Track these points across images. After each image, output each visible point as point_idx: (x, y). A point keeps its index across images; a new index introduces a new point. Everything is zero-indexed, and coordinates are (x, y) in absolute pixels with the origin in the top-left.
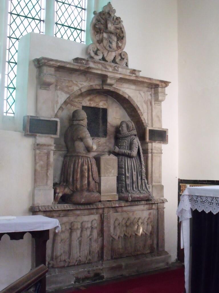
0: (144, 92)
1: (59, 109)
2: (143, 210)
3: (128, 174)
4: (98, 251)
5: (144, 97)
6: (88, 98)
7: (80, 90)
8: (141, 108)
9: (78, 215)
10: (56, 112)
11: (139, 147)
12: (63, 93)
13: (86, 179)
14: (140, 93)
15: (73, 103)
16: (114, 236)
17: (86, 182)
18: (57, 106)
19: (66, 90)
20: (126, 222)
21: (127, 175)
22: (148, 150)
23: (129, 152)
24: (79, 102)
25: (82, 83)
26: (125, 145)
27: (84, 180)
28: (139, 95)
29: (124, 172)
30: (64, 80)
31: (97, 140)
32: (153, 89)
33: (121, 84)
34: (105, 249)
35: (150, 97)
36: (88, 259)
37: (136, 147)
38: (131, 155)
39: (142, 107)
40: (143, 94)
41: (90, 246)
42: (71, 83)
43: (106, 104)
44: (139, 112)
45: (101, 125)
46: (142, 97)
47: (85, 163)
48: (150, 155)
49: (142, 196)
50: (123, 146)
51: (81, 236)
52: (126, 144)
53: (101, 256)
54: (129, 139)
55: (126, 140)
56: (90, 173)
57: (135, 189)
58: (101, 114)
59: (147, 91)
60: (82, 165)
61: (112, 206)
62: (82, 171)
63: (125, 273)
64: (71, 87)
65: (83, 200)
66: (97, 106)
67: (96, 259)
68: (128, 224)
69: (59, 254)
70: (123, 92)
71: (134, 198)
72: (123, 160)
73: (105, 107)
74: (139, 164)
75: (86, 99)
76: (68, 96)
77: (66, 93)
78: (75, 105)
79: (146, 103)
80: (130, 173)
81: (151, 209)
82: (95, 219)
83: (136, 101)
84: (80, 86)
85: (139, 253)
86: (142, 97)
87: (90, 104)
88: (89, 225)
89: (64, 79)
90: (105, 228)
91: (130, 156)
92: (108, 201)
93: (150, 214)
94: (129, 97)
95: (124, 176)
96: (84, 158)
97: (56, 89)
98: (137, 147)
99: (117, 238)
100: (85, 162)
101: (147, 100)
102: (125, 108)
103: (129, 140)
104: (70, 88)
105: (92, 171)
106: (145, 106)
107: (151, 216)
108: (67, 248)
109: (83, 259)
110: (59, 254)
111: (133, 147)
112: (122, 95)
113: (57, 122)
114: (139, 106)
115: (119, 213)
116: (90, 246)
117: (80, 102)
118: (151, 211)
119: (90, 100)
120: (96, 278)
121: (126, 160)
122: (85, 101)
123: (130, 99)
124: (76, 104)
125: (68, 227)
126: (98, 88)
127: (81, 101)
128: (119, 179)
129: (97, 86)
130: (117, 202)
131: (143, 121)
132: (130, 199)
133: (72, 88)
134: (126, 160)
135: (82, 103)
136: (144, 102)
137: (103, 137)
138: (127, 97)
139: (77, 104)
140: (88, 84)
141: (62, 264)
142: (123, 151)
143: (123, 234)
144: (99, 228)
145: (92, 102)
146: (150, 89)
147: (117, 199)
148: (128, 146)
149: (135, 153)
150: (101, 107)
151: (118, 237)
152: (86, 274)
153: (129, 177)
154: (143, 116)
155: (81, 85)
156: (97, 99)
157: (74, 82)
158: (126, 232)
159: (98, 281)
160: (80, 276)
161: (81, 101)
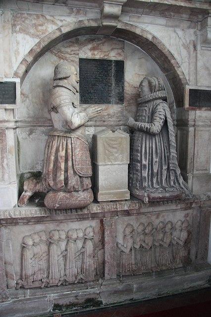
0: (183, 30)
1: (21, 63)
2: (174, 211)
3: (146, 161)
4: (96, 269)
5: (182, 38)
6: (90, 46)
7: (59, 29)
8: (176, 56)
9: (61, 222)
10: (15, 69)
11: (166, 118)
12: (27, 37)
13: (63, 173)
14: (175, 32)
15: (62, 54)
16: (122, 249)
17: (62, 177)
18: (16, 59)
19: (32, 31)
20: (145, 229)
21: (144, 162)
22: (188, 121)
23: (147, 125)
24: (73, 53)
25: (62, 18)
26: (144, 114)
27: (58, 175)
28: (174, 35)
29: (139, 158)
30: (28, 14)
31: (94, 108)
32: (199, 23)
33: (139, 17)
34: (107, 265)
35: (193, 38)
36: (79, 278)
37: (161, 118)
38: (151, 131)
39: (180, 54)
40: (180, 33)
41: (83, 262)
42: (41, 20)
43: (122, 53)
44: (173, 61)
45: (114, 85)
46: (180, 38)
47: (61, 147)
48: (191, 129)
49: (167, 195)
50: (141, 116)
51: (66, 250)
52: (146, 113)
53: (100, 273)
54: (151, 105)
55: (146, 106)
56: (70, 164)
57: (155, 185)
58: (113, 69)
59: (189, 27)
60: (57, 150)
61: (117, 209)
62: (56, 160)
63: (137, 296)
64: (41, 25)
65: (57, 205)
66: (106, 57)
67: (92, 277)
68: (147, 231)
69: (30, 272)
70: (143, 30)
71: (154, 198)
72: (140, 139)
73: (119, 58)
74: (166, 144)
75: (86, 47)
76: (37, 40)
77: (33, 36)
78: (66, 58)
79: (186, 47)
80: (149, 159)
81: (190, 208)
82: (91, 226)
83: (167, 45)
84: (60, 24)
85: (164, 268)
86: (180, 38)
87: (93, 54)
88: (81, 235)
89: (28, 12)
90: (106, 239)
91: (149, 133)
92: (111, 201)
93: (187, 216)
94: (154, 37)
95: (139, 165)
96: (61, 140)
97: (14, 31)
98: (163, 117)
99: (127, 251)
100: (61, 145)
101: (188, 42)
102: (154, 59)
103: (151, 107)
104: (40, 28)
105: (72, 160)
106: (184, 53)
107: (188, 218)
108: (43, 264)
109: (71, 279)
110: (30, 272)
111: (155, 118)
112: (141, 34)
113: (15, 84)
114: (173, 52)
115: (133, 217)
116: (83, 262)
117: (75, 52)
118: (190, 211)
119: (93, 49)
120: (89, 304)
121: (144, 139)
122: (83, 51)
123: (155, 42)
124: (68, 56)
125: (44, 238)
126: (94, 24)
127: (76, 50)
128: (131, 168)
129: (91, 21)
130: (128, 203)
131: (181, 77)
132: (146, 199)
133: (44, 28)
134: (144, 139)
135: (78, 54)
136: (183, 45)
137: (117, 103)
138: (150, 37)
139: (69, 56)
140: (75, 20)
141: (37, 284)
142: (140, 125)
143: (139, 244)
144: (97, 238)
145: (96, 52)
146: (193, 25)
147: (128, 198)
148: (149, 116)
149: (157, 127)
150: (114, 59)
151: (129, 250)
152: (72, 300)
153: (147, 166)
154: (180, 69)
155: (61, 21)
156: (106, 48)
157: (48, 17)
158: (144, 241)
159: (92, 308)
160: (61, 302)
161: (76, 50)
